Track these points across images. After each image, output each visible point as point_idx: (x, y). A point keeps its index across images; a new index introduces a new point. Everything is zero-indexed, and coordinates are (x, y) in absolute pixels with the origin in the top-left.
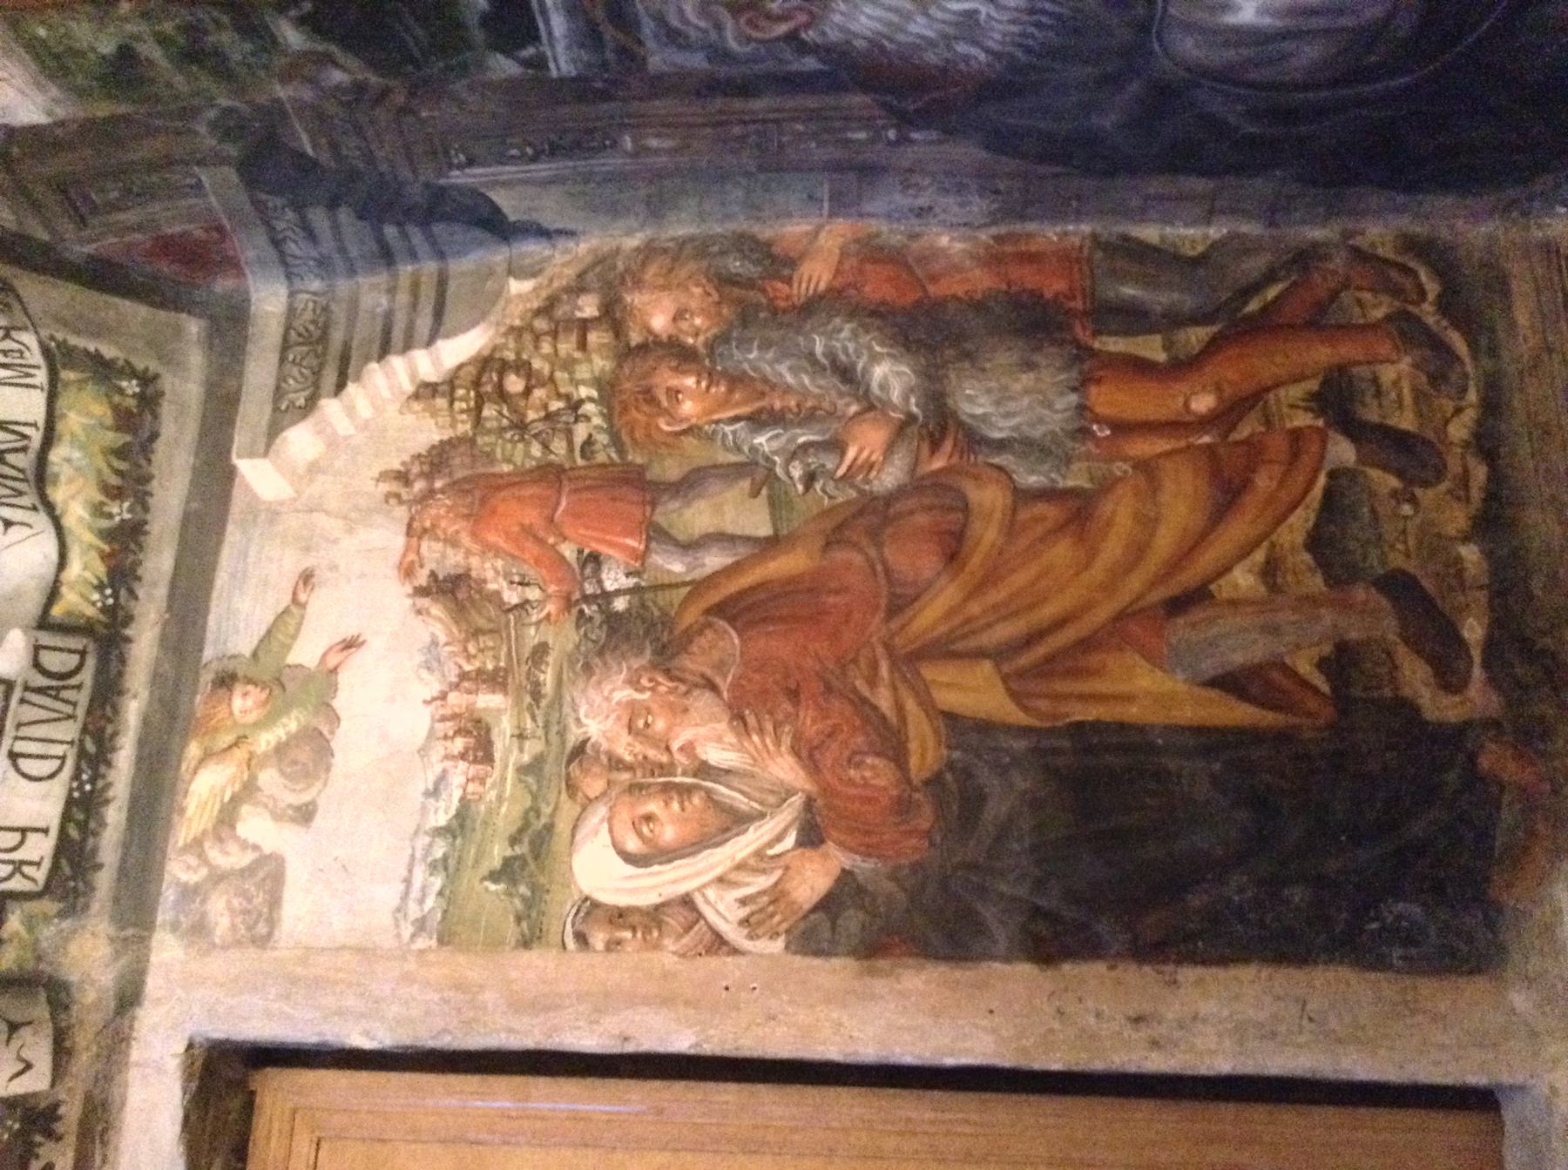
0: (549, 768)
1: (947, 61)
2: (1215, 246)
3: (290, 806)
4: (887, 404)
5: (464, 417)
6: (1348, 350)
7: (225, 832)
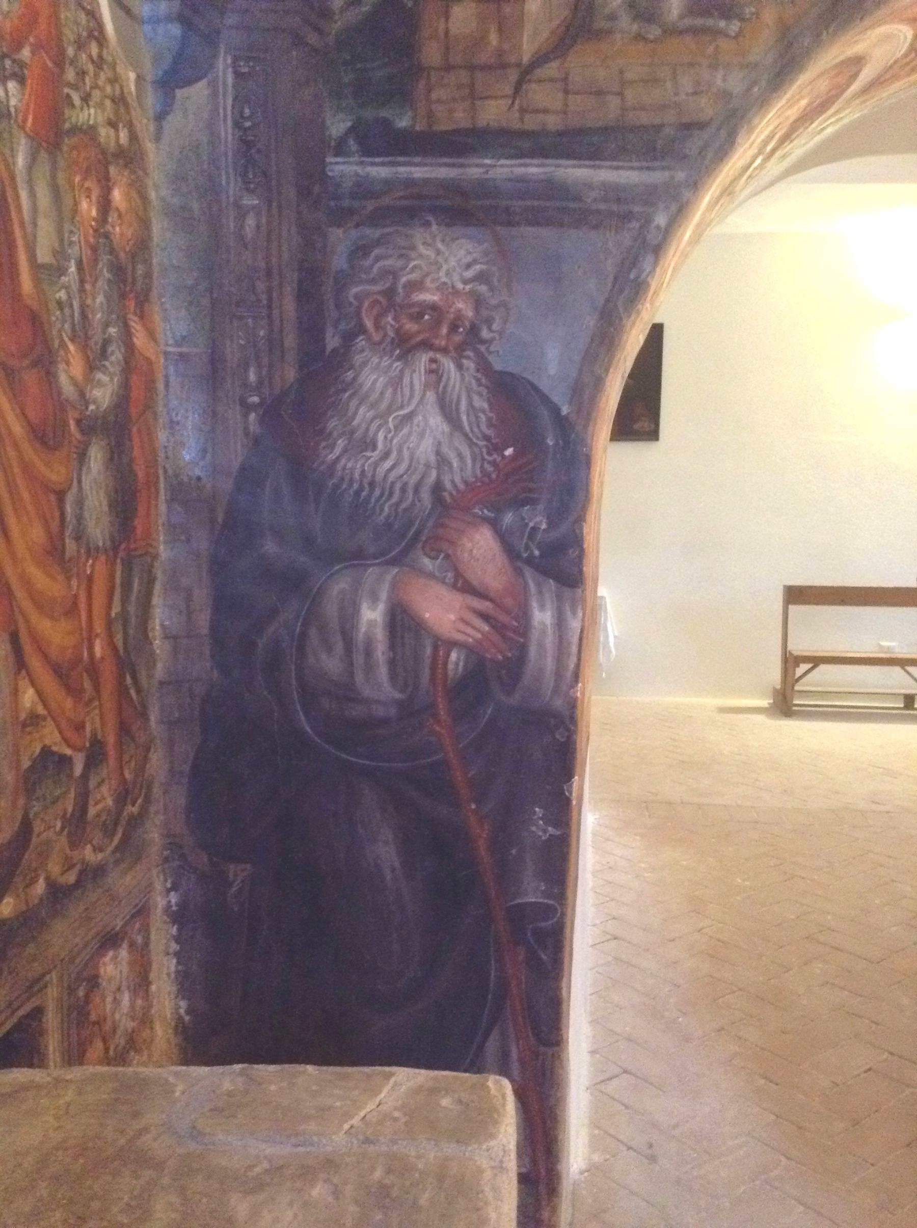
1: (330, 434)
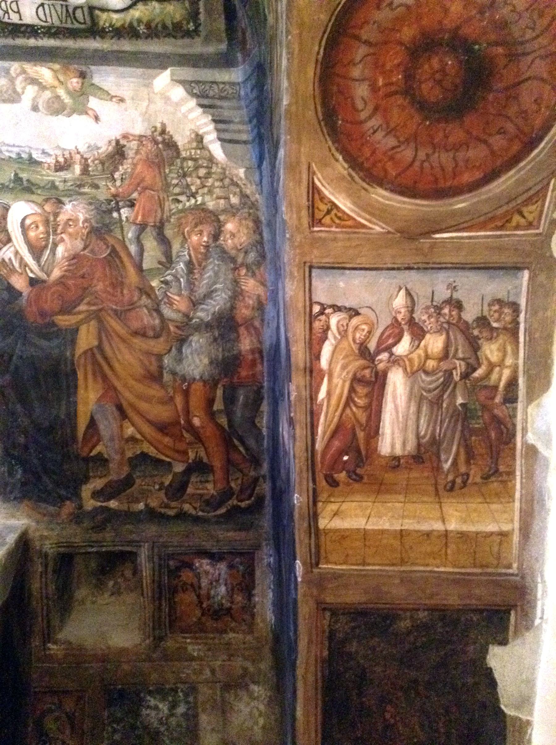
0: (53, 191)
2: (260, 430)
3: (38, 103)
4: (195, 310)
5: (188, 154)
6: (219, 474)
7: (28, 81)
